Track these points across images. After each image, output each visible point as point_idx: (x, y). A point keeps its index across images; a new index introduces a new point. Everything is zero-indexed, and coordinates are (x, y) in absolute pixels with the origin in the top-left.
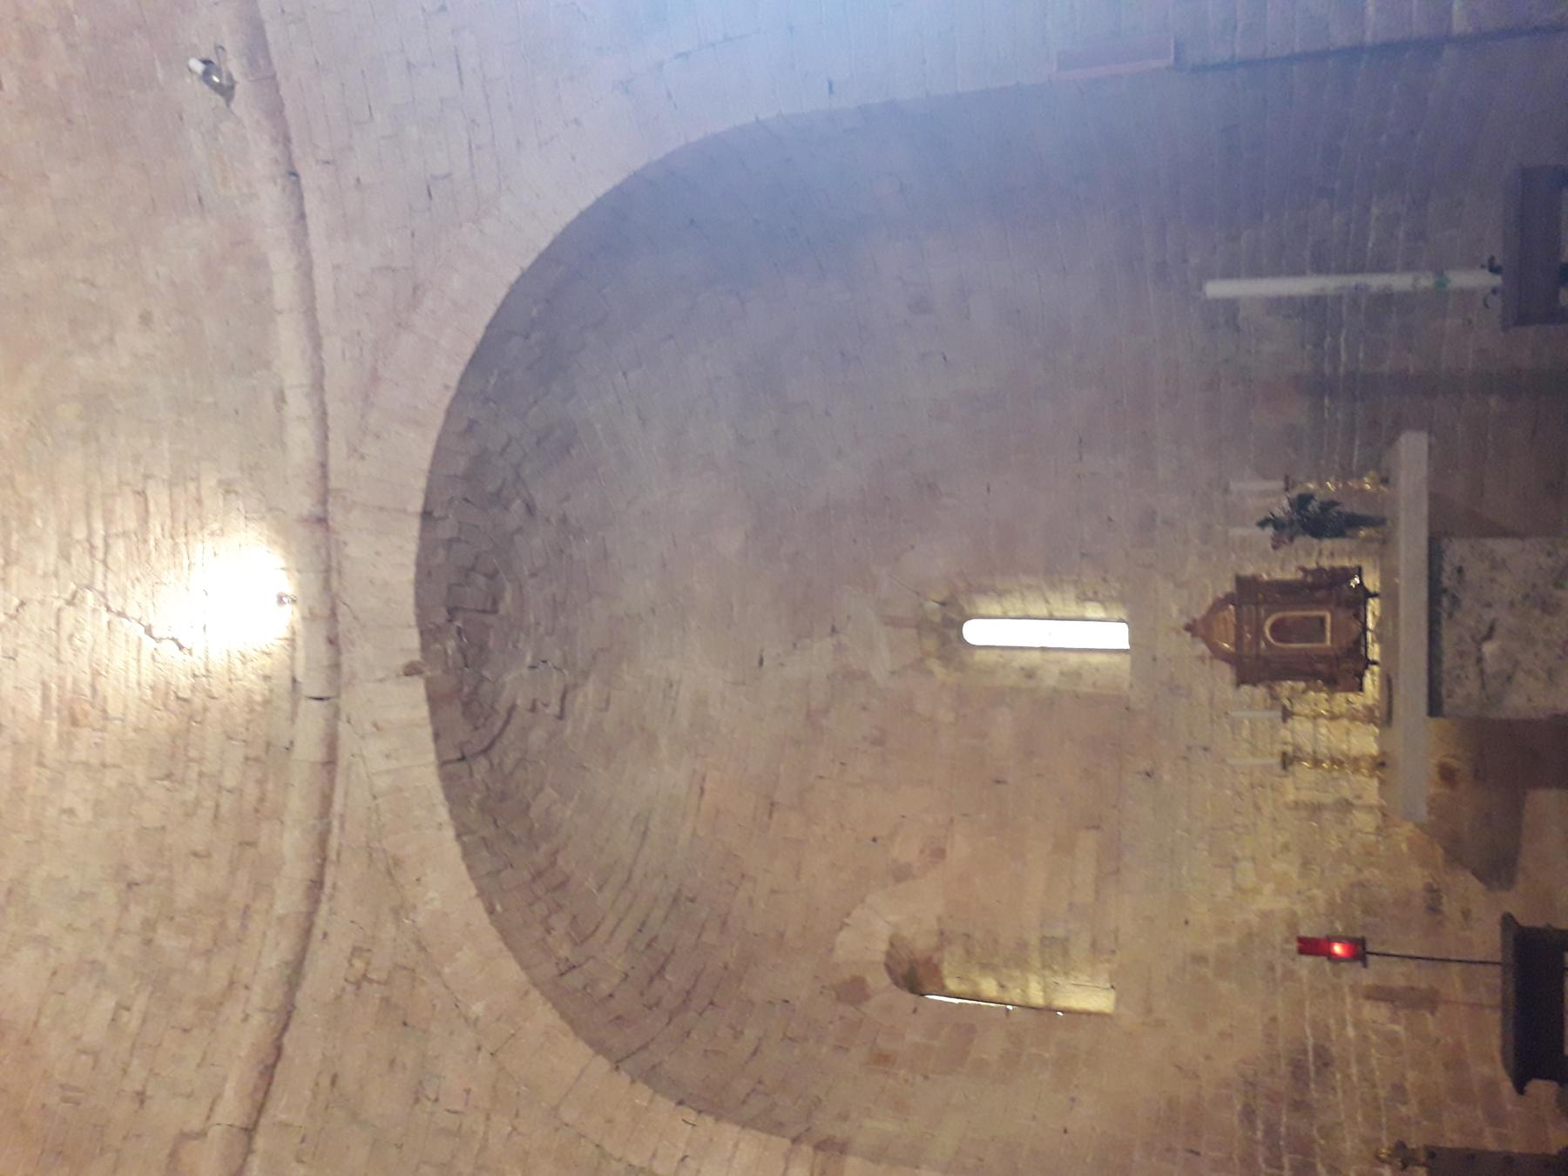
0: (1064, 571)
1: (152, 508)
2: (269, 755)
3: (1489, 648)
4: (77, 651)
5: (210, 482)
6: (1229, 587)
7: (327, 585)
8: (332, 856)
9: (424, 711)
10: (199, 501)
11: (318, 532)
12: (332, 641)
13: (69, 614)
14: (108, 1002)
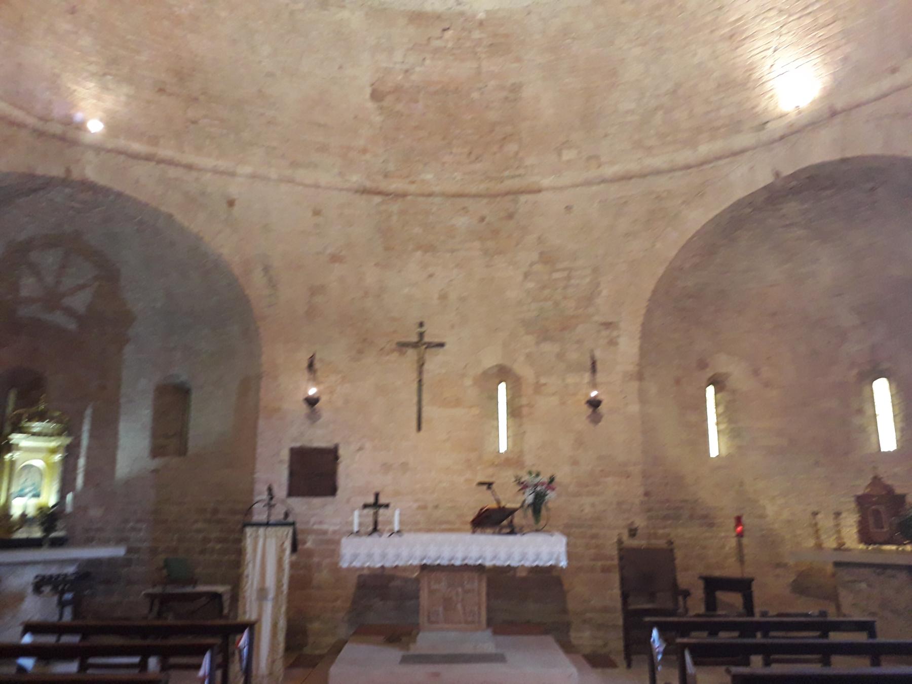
0: (908, 419)
1: (831, 26)
2: (735, 126)
3: (863, 585)
4: (759, 23)
5: (847, 49)
6: (898, 491)
7: (807, 126)
8: (701, 168)
9: (762, 185)
10: (838, 48)
11: (829, 114)
12: (782, 138)
13: (772, 13)
14: (633, 106)
